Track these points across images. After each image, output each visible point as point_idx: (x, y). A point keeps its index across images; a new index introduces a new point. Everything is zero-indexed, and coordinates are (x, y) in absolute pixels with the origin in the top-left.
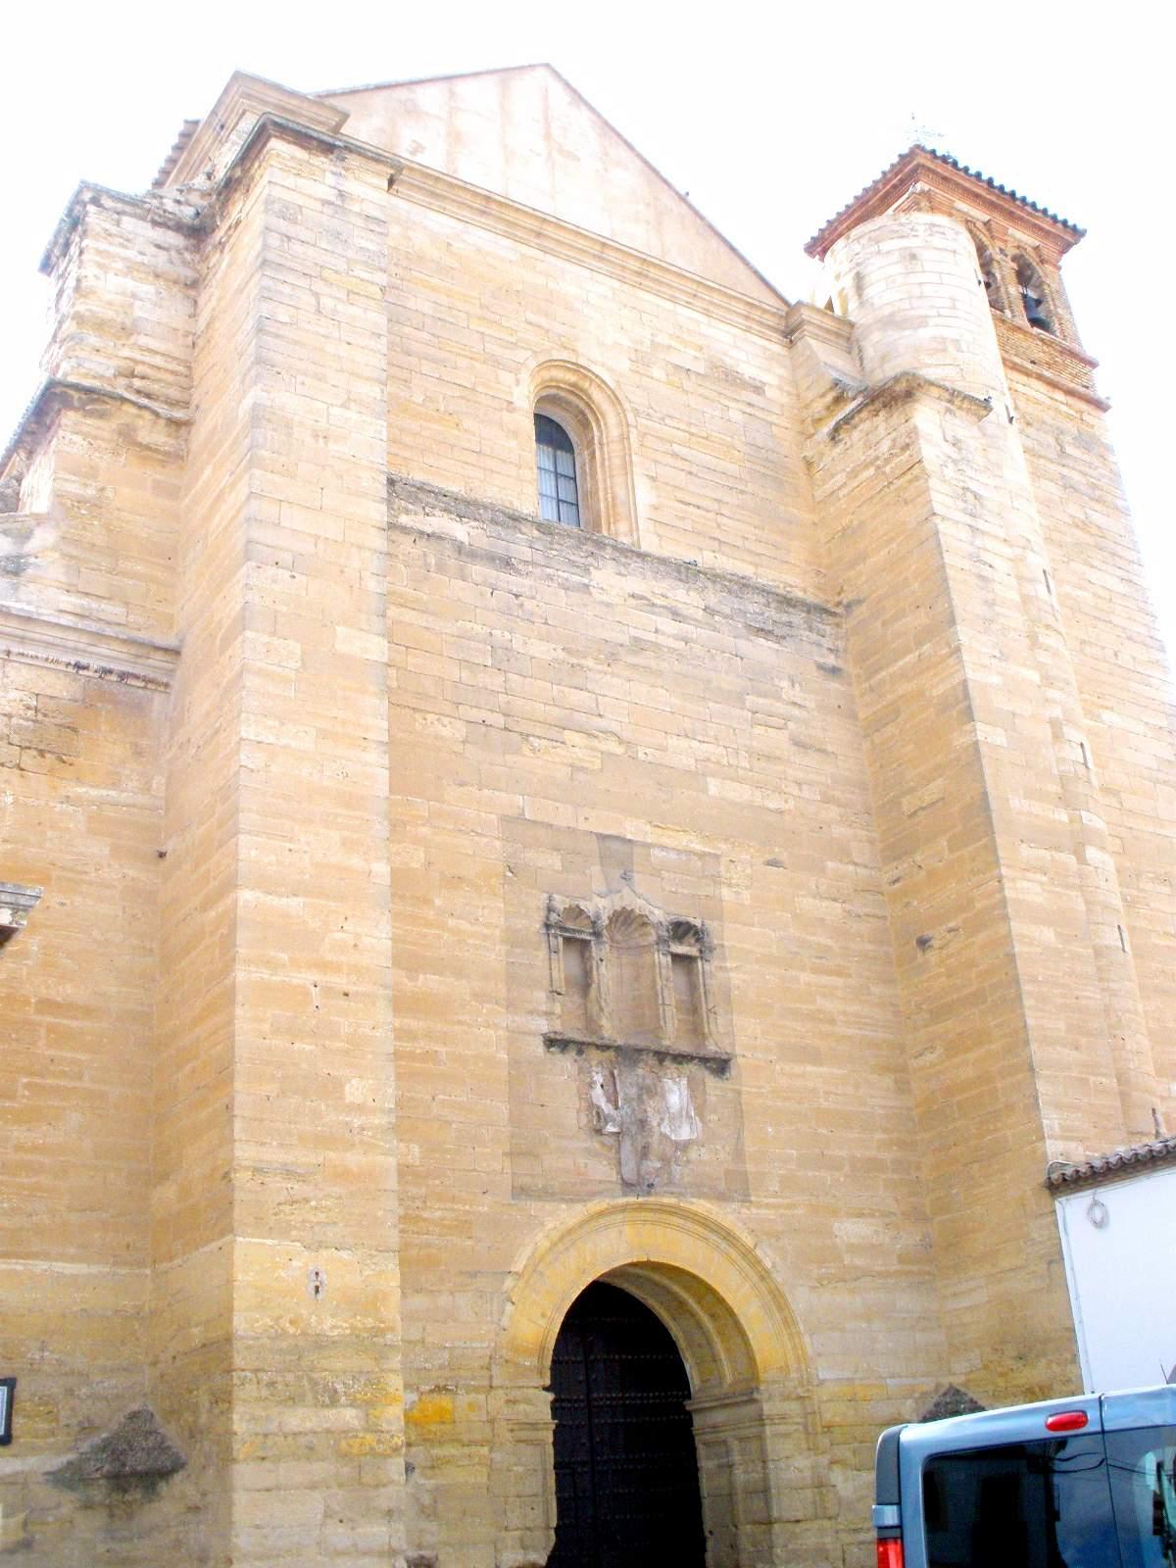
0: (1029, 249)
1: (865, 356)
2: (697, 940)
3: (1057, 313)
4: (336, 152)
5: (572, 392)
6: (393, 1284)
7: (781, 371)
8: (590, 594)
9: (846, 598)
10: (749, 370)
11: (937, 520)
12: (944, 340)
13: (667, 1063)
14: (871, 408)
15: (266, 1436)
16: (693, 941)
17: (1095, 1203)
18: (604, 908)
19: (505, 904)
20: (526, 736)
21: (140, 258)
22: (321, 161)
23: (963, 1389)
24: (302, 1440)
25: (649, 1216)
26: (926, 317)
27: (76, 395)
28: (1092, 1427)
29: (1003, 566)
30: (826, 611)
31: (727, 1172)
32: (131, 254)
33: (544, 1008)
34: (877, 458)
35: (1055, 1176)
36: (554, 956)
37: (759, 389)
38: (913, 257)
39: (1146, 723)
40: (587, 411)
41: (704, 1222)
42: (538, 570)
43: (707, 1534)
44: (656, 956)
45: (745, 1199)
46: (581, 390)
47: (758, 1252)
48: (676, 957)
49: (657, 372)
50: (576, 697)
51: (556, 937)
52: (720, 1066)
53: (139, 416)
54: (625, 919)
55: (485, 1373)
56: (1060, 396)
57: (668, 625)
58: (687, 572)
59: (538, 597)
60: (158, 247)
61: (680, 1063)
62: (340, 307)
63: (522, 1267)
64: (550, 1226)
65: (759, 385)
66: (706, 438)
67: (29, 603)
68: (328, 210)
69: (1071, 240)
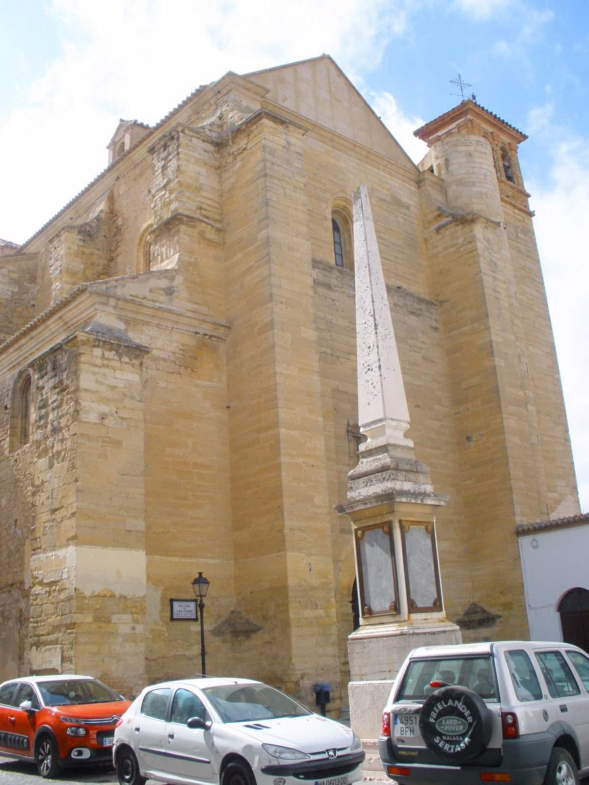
4: (286, 124)
5: (344, 210)
7: (415, 199)
9: (441, 298)
10: (405, 200)
11: (482, 274)
14: (455, 223)
17: (534, 540)
21: (199, 157)
22: (280, 128)
23: (478, 603)
26: (475, 182)
27: (185, 219)
30: (433, 303)
32: (196, 155)
34: (457, 244)
35: (520, 529)
37: (408, 208)
38: (470, 155)
56: (516, 211)
60: (205, 151)
62: (292, 194)
66: (391, 230)
67: (177, 307)
68: (284, 150)
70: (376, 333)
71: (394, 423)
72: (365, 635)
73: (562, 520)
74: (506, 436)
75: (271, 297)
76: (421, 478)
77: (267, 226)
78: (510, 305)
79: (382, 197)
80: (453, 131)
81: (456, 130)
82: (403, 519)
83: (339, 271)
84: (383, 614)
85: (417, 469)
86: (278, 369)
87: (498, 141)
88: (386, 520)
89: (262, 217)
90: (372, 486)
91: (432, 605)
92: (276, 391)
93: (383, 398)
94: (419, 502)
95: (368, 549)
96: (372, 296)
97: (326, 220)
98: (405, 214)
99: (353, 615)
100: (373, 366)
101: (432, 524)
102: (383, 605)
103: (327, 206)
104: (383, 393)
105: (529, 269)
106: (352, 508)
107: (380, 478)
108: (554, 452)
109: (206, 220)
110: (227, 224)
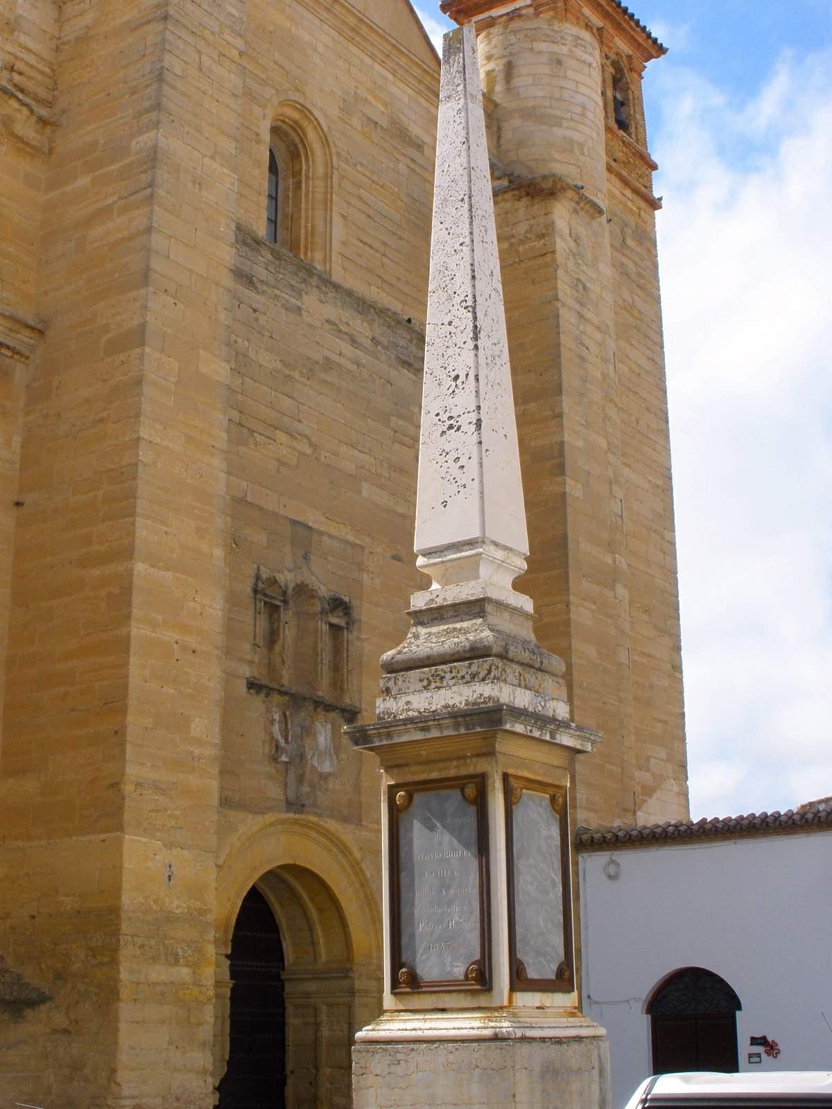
0: (624, 57)
1: (503, 135)
2: (345, 614)
3: (635, 117)
6: (212, 877)
8: (301, 315)
11: (559, 305)
12: (571, 141)
14: (516, 192)
15: (138, 984)
16: (341, 614)
17: (612, 861)
20: (252, 431)
24: (159, 988)
26: (561, 118)
28: (281, 973)
29: (594, 348)
33: (249, 657)
34: (513, 236)
35: (584, 837)
36: (258, 616)
38: (559, 62)
39: (650, 481)
40: (300, 146)
41: (327, 834)
42: (269, 291)
43: (288, 1073)
44: (320, 624)
46: (300, 127)
47: (363, 865)
48: (332, 626)
49: (356, 122)
50: (287, 403)
51: (260, 601)
53: (18, 110)
56: (628, 193)
57: (347, 349)
58: (364, 306)
59: (268, 313)
61: (327, 711)
65: (420, 142)
66: (382, 186)
69: (655, 54)
70: (476, 347)
71: (500, 554)
72: (400, 1034)
73: (676, 826)
74: (573, 641)
75: (145, 277)
76: (549, 684)
77: (157, 125)
78: (605, 376)
79: (372, 118)
80: (524, 12)
81: (531, 10)
82: (510, 771)
83: (273, 252)
84: (445, 987)
85: (542, 663)
86: (144, 433)
87: (610, 48)
88: (471, 770)
89: (147, 104)
90: (443, 691)
91: (553, 977)
92: (135, 478)
93: (482, 493)
94: (548, 738)
95: (419, 836)
96: (472, 265)
97: (258, 142)
98: (413, 160)
99: (231, 985)
100: (463, 421)
101: (563, 792)
102: (448, 969)
103: (264, 116)
104: (481, 482)
105: (640, 312)
106: (389, 736)
107: (463, 672)
108: (651, 687)
109: (21, 96)
110: (64, 112)
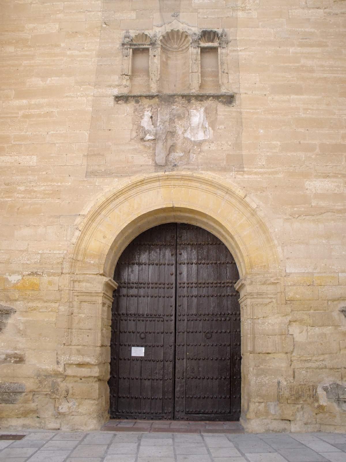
13: (193, 101)
18: (159, 32)
19: (100, 39)
25: (177, 182)
31: (228, 155)
45: (240, 169)
47: (247, 199)
52: (229, 99)
54: (173, 37)
55: (60, 266)
63: (87, 212)
64: (107, 190)
